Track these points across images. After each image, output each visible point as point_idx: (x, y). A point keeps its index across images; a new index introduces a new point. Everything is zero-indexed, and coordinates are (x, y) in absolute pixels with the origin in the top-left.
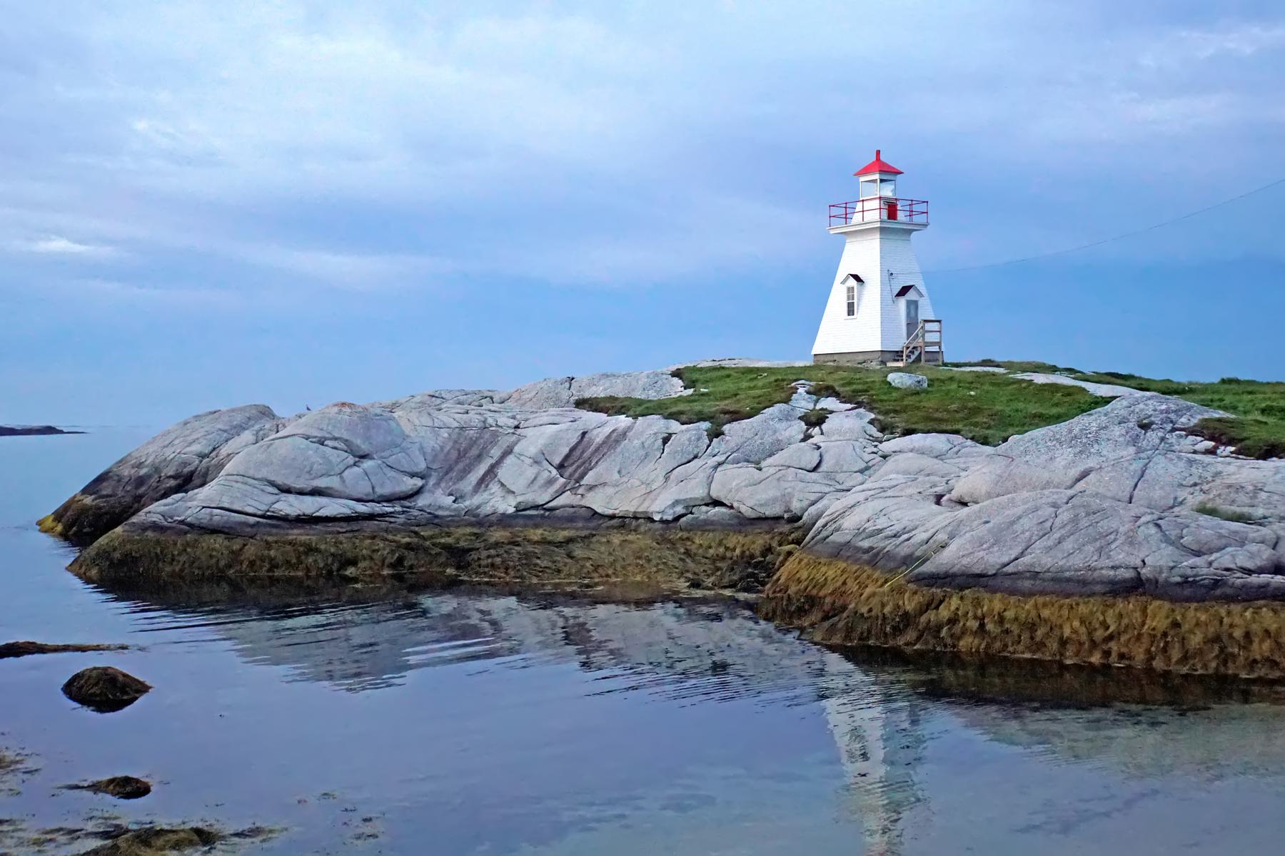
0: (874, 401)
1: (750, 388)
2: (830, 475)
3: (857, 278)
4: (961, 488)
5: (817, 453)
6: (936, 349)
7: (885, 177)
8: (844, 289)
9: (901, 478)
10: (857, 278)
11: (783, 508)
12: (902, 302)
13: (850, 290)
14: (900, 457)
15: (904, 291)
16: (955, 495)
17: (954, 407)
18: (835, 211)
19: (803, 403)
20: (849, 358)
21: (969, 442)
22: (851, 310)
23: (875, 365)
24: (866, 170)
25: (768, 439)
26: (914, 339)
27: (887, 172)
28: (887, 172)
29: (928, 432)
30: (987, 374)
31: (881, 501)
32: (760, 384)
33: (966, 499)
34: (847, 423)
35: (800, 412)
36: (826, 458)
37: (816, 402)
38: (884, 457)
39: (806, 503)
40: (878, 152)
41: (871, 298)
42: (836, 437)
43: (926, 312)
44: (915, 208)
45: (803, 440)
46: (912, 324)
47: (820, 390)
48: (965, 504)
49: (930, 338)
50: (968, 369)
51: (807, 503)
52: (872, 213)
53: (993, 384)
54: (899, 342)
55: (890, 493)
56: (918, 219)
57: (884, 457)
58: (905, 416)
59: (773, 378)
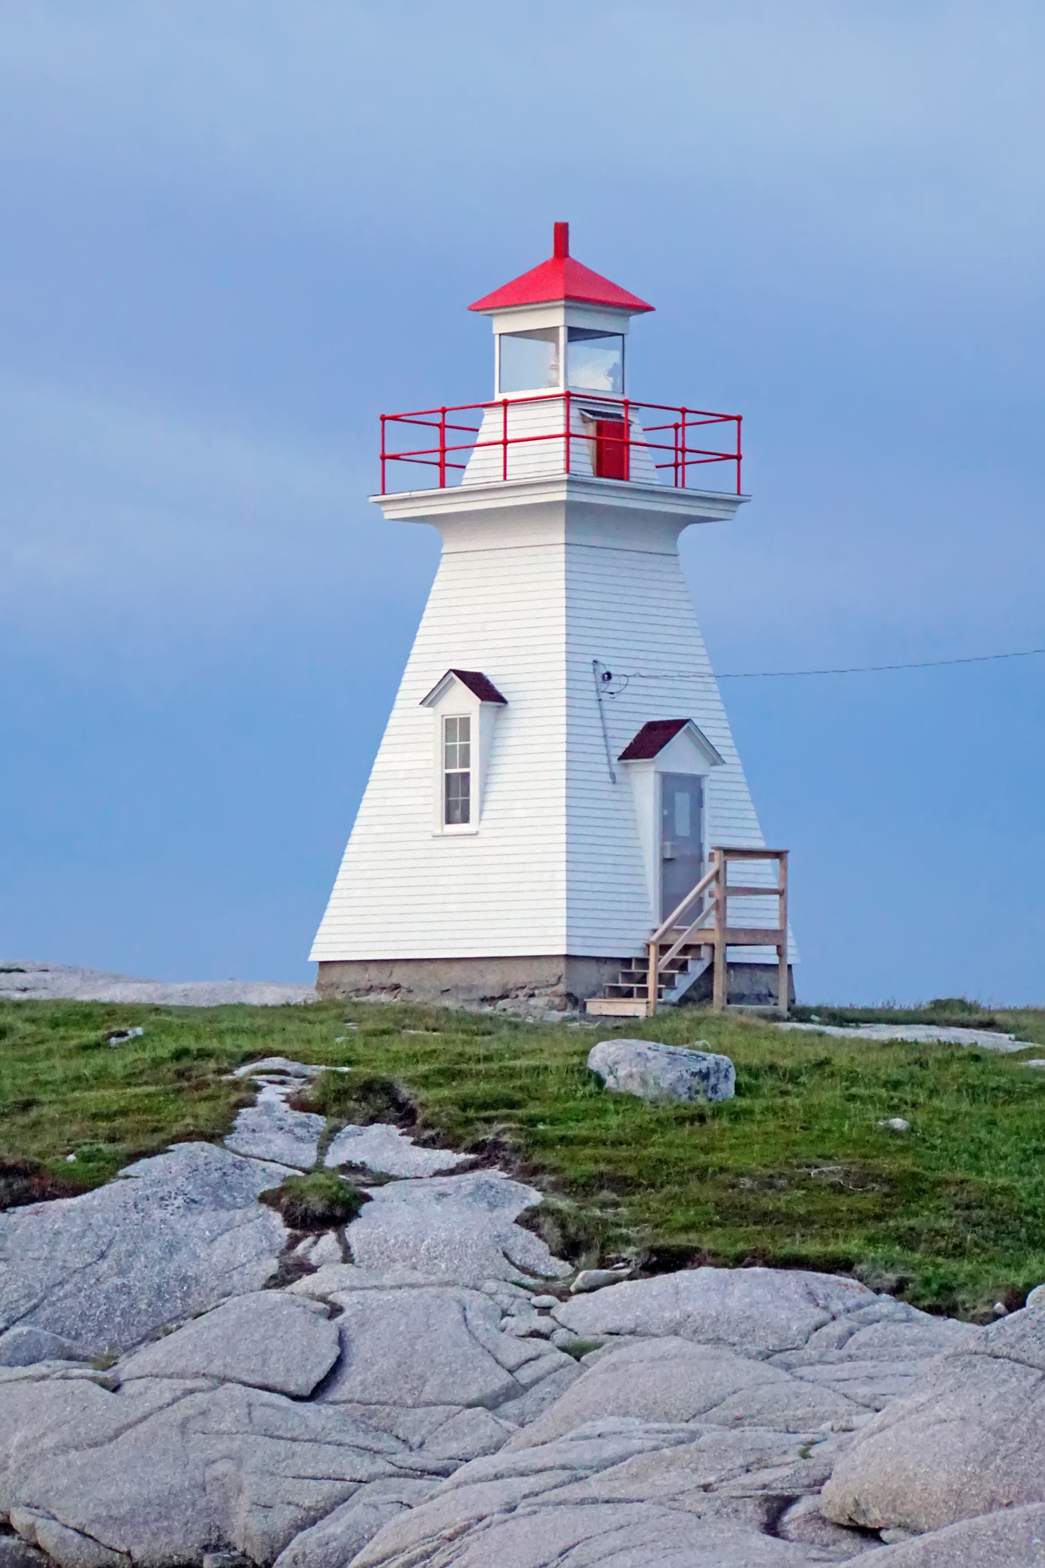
0: (544, 1143)
1: (78, 1081)
2: (368, 1414)
3: (479, 685)
4: (857, 1475)
5: (327, 1330)
6: (767, 954)
7: (585, 321)
8: (432, 721)
9: (637, 1433)
10: (479, 685)
11: (199, 1535)
12: (645, 778)
13: (456, 728)
14: (635, 1349)
15: (652, 739)
16: (833, 1499)
17: (832, 1171)
18: (400, 439)
19: (280, 1144)
20: (456, 973)
21: (886, 1304)
22: (456, 804)
23: (541, 1008)
24: (520, 293)
25: (142, 1274)
26: (687, 917)
27: (573, 286)
28: (573, 286)
29: (739, 1261)
30: (951, 1052)
31: (567, 1516)
32: (118, 1067)
33: (874, 1517)
34: (438, 1221)
35: (268, 1177)
36: (361, 1348)
37: (329, 1137)
38: (577, 1351)
39: (283, 1517)
40: (561, 232)
41: (535, 760)
42: (399, 1272)
43: (731, 816)
44: (694, 438)
45: (278, 1281)
46: (680, 863)
47: (341, 1096)
48: (871, 1534)
49: (745, 913)
50: (883, 1033)
51: (290, 1514)
52: (531, 447)
53: (975, 1093)
54: (633, 927)
55: (594, 1487)
56: (701, 478)
57: (577, 1351)
58: (654, 1199)
59: (166, 1047)
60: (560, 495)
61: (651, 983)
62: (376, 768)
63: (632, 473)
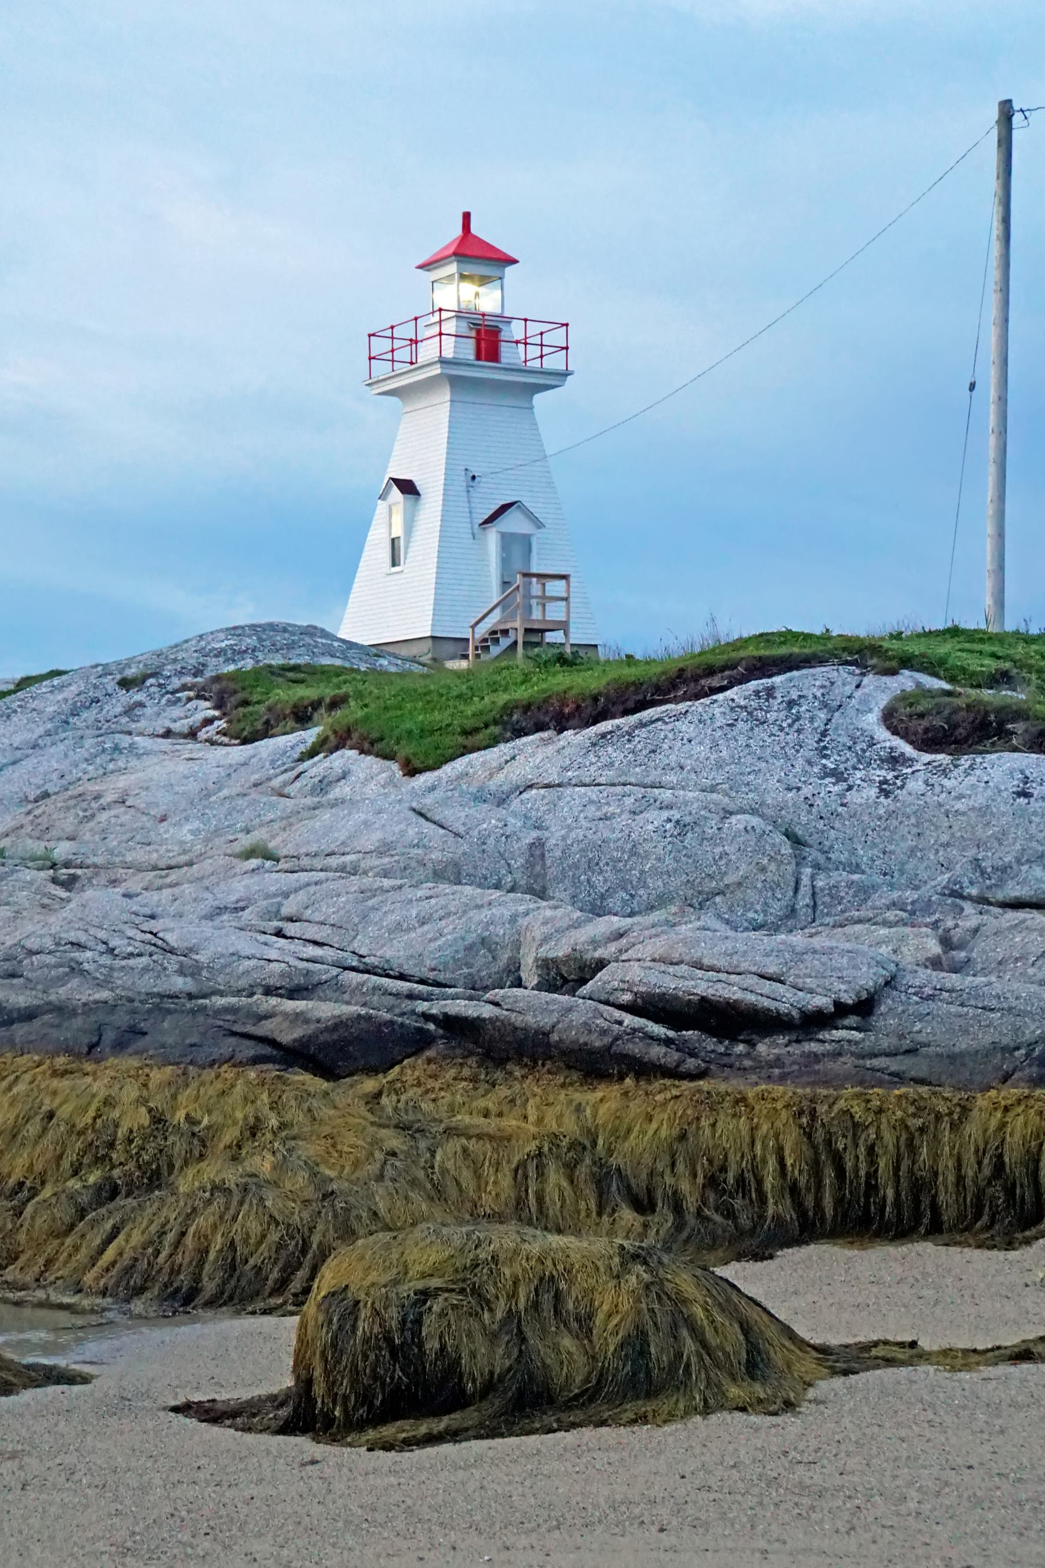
12: (492, 538)
40: (467, 217)
60: (437, 370)
61: (471, 652)
62: (369, 538)
63: (503, 360)
